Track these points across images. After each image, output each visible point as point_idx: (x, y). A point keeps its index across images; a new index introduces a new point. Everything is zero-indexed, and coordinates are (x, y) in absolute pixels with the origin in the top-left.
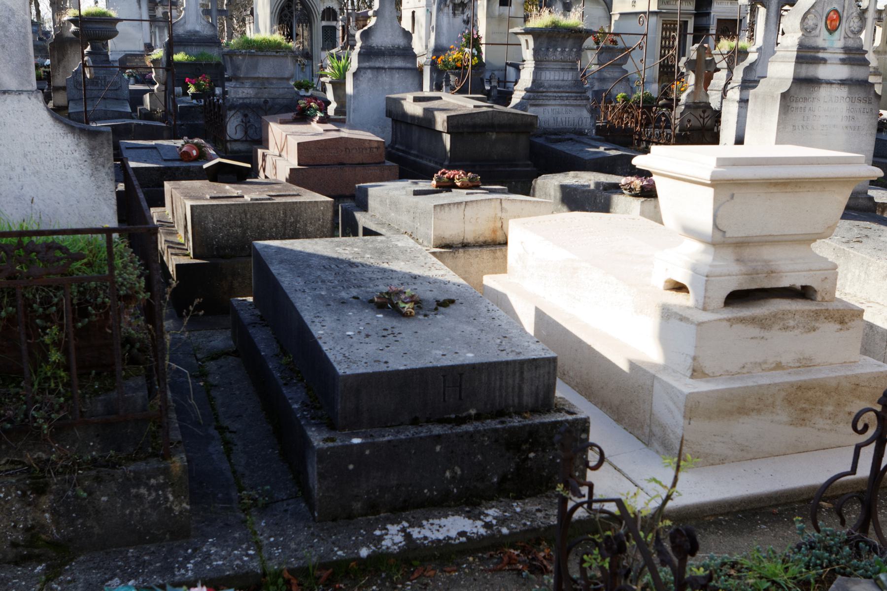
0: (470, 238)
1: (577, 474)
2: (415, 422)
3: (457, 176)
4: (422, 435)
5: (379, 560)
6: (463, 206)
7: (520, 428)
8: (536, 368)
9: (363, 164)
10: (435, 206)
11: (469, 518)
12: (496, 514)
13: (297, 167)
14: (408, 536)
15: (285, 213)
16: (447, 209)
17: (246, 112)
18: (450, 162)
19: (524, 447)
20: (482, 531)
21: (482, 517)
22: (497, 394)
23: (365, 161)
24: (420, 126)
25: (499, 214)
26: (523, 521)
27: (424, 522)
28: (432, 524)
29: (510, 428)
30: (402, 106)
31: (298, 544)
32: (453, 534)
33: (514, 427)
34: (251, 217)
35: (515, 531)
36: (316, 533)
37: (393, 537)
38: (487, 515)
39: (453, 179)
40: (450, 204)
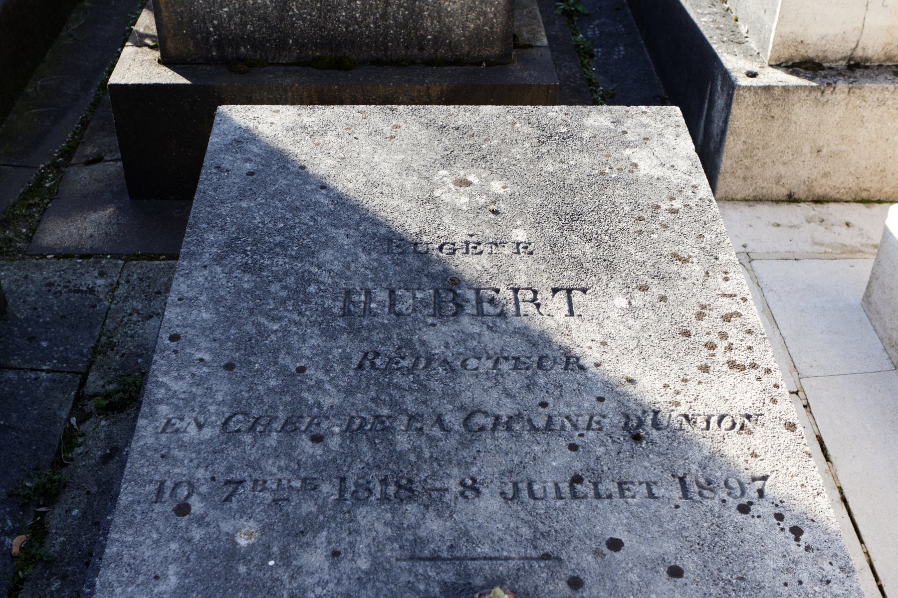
0: (873, 47)
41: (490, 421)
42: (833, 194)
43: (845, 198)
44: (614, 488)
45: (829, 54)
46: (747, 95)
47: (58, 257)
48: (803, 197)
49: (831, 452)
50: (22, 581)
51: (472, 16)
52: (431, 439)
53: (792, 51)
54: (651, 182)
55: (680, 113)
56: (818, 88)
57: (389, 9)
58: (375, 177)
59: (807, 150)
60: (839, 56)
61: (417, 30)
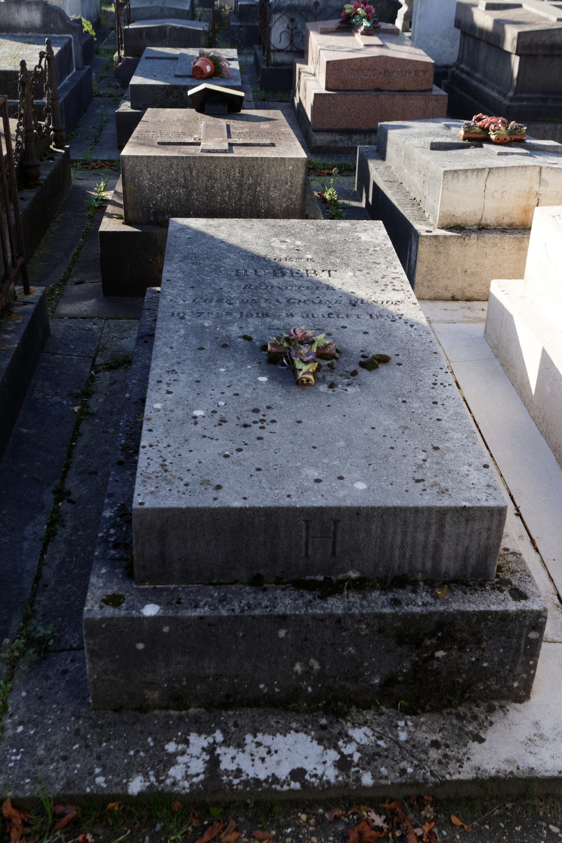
0: (490, 218)
1: (516, 684)
2: (257, 582)
3: (492, 127)
4: (257, 612)
5: (156, 803)
6: (485, 174)
7: (422, 616)
8: (467, 521)
9: (404, 91)
10: (446, 172)
11: (320, 742)
12: (365, 741)
13: (324, 91)
14: (213, 763)
15: (242, 173)
16: (462, 177)
17: (294, 16)
18: (515, 93)
19: (428, 642)
20: (331, 774)
21: (340, 743)
22: (397, 552)
23: (407, 88)
24: (489, 44)
25: (536, 188)
26: (403, 764)
27: (249, 738)
28: (259, 744)
29: (406, 615)
30: (471, 15)
31: (48, 750)
32: (283, 773)
33: (413, 615)
34: (198, 175)
35: (383, 782)
36: (82, 732)
37: (188, 764)
38: (350, 740)
39: (487, 130)
40: (466, 171)
41: (297, 301)
42: (475, 296)
43: (482, 298)
44: (345, 316)
45: (468, 222)
46: (426, 240)
47: (70, 318)
48: (460, 298)
49: (460, 385)
50: (82, 420)
51: (285, 200)
52: (274, 305)
53: (449, 220)
54: (366, 242)
55: (384, 232)
56: (462, 237)
57: (243, 196)
58: (244, 239)
59: (459, 271)
60: (473, 224)
61: (256, 207)
